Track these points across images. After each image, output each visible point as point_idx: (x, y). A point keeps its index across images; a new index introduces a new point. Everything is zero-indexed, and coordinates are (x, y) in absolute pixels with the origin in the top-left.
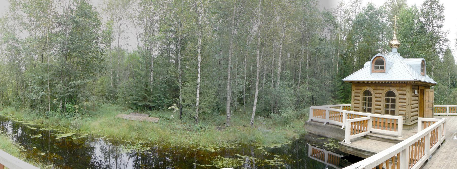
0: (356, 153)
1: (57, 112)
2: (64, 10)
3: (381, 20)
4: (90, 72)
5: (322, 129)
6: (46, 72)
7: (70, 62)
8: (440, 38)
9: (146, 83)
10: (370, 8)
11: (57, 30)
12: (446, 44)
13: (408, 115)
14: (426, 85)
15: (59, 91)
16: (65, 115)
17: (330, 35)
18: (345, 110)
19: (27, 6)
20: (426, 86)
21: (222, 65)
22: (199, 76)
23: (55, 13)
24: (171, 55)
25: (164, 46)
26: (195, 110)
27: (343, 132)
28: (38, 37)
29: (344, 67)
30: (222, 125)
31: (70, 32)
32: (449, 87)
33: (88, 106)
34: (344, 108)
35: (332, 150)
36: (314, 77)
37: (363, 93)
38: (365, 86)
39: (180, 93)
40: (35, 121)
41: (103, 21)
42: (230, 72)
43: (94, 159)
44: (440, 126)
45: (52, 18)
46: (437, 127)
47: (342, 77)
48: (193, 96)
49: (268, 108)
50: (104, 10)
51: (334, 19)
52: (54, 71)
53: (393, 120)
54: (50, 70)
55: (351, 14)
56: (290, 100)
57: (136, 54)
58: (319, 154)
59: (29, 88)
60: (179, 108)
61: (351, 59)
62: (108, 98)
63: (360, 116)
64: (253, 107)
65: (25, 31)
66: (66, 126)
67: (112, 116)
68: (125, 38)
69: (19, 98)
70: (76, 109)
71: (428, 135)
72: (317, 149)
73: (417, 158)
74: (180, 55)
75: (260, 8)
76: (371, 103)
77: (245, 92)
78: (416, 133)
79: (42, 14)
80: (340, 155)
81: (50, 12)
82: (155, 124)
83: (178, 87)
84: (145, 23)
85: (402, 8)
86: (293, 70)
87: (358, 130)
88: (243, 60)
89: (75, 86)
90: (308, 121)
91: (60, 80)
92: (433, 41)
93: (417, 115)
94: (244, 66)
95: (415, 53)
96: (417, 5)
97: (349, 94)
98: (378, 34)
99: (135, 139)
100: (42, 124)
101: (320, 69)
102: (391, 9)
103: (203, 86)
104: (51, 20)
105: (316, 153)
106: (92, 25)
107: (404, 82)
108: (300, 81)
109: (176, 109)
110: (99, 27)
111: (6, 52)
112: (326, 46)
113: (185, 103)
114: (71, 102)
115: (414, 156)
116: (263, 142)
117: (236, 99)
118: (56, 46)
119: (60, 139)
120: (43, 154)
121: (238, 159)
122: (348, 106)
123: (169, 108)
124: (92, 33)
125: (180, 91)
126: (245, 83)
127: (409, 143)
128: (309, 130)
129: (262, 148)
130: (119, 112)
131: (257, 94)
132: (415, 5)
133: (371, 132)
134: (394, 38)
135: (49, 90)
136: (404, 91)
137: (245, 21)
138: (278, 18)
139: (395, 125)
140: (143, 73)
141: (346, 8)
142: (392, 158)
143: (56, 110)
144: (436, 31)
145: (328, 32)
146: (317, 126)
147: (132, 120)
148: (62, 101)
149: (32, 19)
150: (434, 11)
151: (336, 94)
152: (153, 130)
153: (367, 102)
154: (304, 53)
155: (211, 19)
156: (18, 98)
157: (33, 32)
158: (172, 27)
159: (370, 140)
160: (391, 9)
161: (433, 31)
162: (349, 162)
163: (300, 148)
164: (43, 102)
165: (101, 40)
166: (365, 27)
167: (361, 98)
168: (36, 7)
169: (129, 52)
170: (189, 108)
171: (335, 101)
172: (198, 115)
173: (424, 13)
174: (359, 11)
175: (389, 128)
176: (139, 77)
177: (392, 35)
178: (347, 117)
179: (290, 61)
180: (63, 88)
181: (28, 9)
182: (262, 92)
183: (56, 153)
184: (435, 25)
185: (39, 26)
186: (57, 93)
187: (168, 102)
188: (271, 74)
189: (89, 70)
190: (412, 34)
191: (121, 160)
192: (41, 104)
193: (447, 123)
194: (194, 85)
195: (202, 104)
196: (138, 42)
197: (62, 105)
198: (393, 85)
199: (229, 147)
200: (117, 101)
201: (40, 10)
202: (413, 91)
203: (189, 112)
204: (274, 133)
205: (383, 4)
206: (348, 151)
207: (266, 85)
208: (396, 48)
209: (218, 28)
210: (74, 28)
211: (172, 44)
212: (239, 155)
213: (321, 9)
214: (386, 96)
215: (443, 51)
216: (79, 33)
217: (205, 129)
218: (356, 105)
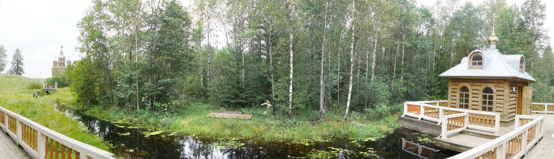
0: (452, 148)
1: (145, 111)
2: (153, 10)
3: (479, 17)
4: (180, 70)
5: (417, 124)
6: (135, 70)
7: (159, 60)
8: (540, 35)
9: (237, 80)
10: (468, 6)
11: (146, 29)
12: (547, 41)
13: (505, 112)
14: (525, 82)
15: (148, 89)
16: (154, 114)
17: (427, 30)
18: (442, 106)
19: (115, 7)
20: (525, 83)
21: (314, 60)
22: (292, 72)
23: (144, 13)
24: (262, 51)
25: (255, 43)
26: (288, 106)
27: (440, 128)
28: (126, 35)
29: (441, 63)
30: (315, 120)
31: (159, 31)
32: (548, 85)
33: (177, 105)
34: (440, 104)
35: (426, 144)
36: (409, 72)
37: (460, 89)
38: (462, 82)
39: (273, 89)
40: (124, 119)
41: (193, 20)
42: (324, 66)
43: (183, 155)
44: (538, 124)
45: (140, 18)
46: (534, 125)
47: (438, 72)
48: (286, 92)
49: (362, 102)
50: (194, 10)
51: (431, 15)
52: (143, 69)
53: (491, 117)
54: (138, 68)
55: (448, 12)
56: (385, 95)
57: (226, 51)
58: (413, 148)
59: (117, 86)
60: (272, 104)
61: (448, 55)
62: (198, 97)
63: (457, 113)
64: (347, 102)
65: (112, 30)
66: (155, 125)
67: (203, 115)
68: (214, 36)
69: (107, 96)
70: (165, 108)
71: (525, 132)
72: (411, 143)
73: (514, 153)
74: (271, 50)
75: (354, 5)
76: (468, 100)
77: (338, 86)
78: (513, 129)
79: (130, 14)
80: (436, 149)
81: (138, 12)
82: (248, 121)
83: (271, 83)
84: (234, 21)
85: (501, 7)
86: (388, 65)
87: (455, 126)
88: (336, 54)
89: (164, 84)
90: (403, 116)
91: (149, 78)
92: (533, 38)
93: (515, 112)
94: (338, 61)
95: (514, 49)
96: (517, 4)
97: (445, 91)
98: (477, 30)
99: (229, 136)
100: (131, 122)
101: (415, 64)
102: (491, 7)
103: (296, 81)
104: (140, 19)
105: (409, 147)
106: (182, 24)
107: (502, 79)
108: (395, 76)
109: (270, 105)
110: (190, 26)
111: (93, 50)
112: (423, 41)
113: (277, 99)
114: (160, 101)
115: (511, 151)
116: (356, 136)
117: (329, 94)
118: (145, 44)
119: (149, 136)
120: (131, 151)
121: (332, 152)
122: (445, 103)
123: (262, 104)
124: (182, 31)
125: (273, 87)
126: (339, 78)
127: (506, 139)
128: (404, 125)
129: (356, 141)
130: (211, 111)
131: (351, 88)
132: (515, 5)
133: (468, 128)
134: (492, 35)
135: (138, 89)
136: (502, 87)
137: (338, 16)
138: (373, 13)
139: (492, 122)
140: (234, 70)
141: (442, 6)
142: (489, 152)
143: (144, 108)
144: (537, 28)
145: (425, 27)
146: (412, 121)
147: (225, 118)
148: (150, 100)
149: (120, 18)
150: (535, 10)
151: (432, 90)
152: (247, 126)
153: (464, 98)
154: (400, 47)
155: (303, 15)
156: (106, 96)
157: (121, 31)
158: (262, 23)
159: (467, 135)
160: (490, 8)
161: (533, 29)
162: (445, 156)
163: (394, 141)
164: (132, 101)
165: (191, 38)
166: (462, 23)
167: (458, 95)
168: (124, 8)
169: (219, 49)
170: (282, 104)
171: (431, 97)
172: (292, 111)
173: (525, 11)
174: (457, 9)
175: (486, 124)
176: (230, 74)
177: (491, 32)
178: (443, 113)
179: (385, 55)
180: (151, 87)
181: (115, 9)
182: (356, 86)
183: (145, 150)
184: (535, 23)
185: (127, 24)
186: (145, 91)
187: (260, 98)
188: (366, 68)
189: (178, 68)
190: (511, 31)
191: (212, 157)
192: (130, 103)
193: (545, 121)
194: (287, 81)
195: (295, 99)
196: (227, 39)
197: (150, 104)
199: (323, 141)
200: (208, 100)
201: (128, 11)
202: (511, 88)
203: (282, 108)
204: (368, 127)
205: (482, 3)
207: (360, 80)
208: (494, 44)
209: (309, 23)
210: (163, 27)
211: (263, 39)
212: (333, 148)
213: (419, 6)
214: (483, 93)
215: (543, 48)
216: (169, 31)
217: (299, 124)
218: (453, 101)
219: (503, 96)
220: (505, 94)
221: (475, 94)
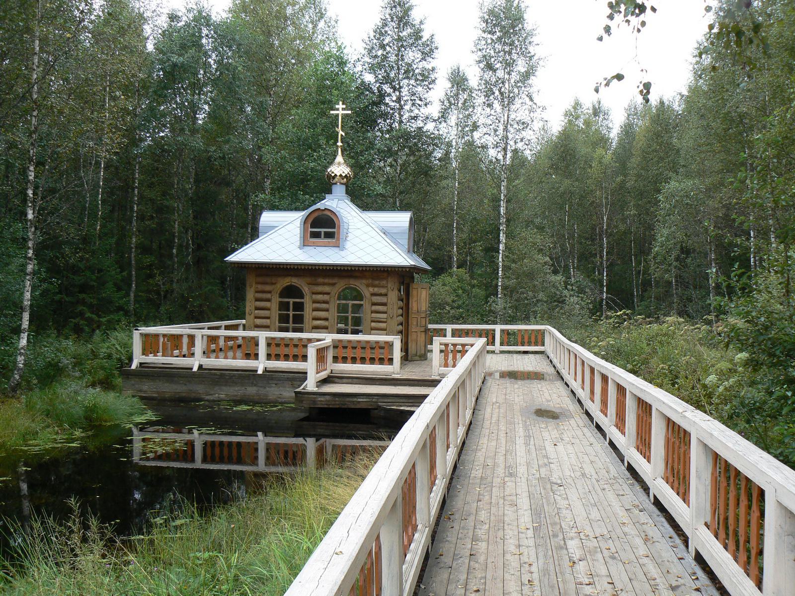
0: (337, 403)
76: (302, 316)
128: (141, 391)
136: (383, 287)
167: (274, 305)
198: (357, 274)
206: (319, 403)
208: (342, 184)
219: (384, 304)
220: (389, 301)
221: (318, 302)
